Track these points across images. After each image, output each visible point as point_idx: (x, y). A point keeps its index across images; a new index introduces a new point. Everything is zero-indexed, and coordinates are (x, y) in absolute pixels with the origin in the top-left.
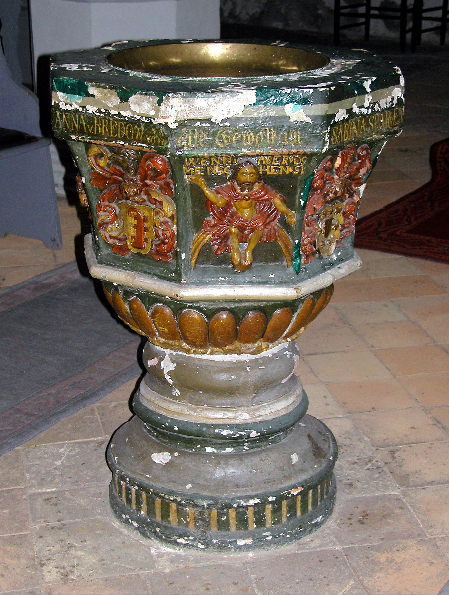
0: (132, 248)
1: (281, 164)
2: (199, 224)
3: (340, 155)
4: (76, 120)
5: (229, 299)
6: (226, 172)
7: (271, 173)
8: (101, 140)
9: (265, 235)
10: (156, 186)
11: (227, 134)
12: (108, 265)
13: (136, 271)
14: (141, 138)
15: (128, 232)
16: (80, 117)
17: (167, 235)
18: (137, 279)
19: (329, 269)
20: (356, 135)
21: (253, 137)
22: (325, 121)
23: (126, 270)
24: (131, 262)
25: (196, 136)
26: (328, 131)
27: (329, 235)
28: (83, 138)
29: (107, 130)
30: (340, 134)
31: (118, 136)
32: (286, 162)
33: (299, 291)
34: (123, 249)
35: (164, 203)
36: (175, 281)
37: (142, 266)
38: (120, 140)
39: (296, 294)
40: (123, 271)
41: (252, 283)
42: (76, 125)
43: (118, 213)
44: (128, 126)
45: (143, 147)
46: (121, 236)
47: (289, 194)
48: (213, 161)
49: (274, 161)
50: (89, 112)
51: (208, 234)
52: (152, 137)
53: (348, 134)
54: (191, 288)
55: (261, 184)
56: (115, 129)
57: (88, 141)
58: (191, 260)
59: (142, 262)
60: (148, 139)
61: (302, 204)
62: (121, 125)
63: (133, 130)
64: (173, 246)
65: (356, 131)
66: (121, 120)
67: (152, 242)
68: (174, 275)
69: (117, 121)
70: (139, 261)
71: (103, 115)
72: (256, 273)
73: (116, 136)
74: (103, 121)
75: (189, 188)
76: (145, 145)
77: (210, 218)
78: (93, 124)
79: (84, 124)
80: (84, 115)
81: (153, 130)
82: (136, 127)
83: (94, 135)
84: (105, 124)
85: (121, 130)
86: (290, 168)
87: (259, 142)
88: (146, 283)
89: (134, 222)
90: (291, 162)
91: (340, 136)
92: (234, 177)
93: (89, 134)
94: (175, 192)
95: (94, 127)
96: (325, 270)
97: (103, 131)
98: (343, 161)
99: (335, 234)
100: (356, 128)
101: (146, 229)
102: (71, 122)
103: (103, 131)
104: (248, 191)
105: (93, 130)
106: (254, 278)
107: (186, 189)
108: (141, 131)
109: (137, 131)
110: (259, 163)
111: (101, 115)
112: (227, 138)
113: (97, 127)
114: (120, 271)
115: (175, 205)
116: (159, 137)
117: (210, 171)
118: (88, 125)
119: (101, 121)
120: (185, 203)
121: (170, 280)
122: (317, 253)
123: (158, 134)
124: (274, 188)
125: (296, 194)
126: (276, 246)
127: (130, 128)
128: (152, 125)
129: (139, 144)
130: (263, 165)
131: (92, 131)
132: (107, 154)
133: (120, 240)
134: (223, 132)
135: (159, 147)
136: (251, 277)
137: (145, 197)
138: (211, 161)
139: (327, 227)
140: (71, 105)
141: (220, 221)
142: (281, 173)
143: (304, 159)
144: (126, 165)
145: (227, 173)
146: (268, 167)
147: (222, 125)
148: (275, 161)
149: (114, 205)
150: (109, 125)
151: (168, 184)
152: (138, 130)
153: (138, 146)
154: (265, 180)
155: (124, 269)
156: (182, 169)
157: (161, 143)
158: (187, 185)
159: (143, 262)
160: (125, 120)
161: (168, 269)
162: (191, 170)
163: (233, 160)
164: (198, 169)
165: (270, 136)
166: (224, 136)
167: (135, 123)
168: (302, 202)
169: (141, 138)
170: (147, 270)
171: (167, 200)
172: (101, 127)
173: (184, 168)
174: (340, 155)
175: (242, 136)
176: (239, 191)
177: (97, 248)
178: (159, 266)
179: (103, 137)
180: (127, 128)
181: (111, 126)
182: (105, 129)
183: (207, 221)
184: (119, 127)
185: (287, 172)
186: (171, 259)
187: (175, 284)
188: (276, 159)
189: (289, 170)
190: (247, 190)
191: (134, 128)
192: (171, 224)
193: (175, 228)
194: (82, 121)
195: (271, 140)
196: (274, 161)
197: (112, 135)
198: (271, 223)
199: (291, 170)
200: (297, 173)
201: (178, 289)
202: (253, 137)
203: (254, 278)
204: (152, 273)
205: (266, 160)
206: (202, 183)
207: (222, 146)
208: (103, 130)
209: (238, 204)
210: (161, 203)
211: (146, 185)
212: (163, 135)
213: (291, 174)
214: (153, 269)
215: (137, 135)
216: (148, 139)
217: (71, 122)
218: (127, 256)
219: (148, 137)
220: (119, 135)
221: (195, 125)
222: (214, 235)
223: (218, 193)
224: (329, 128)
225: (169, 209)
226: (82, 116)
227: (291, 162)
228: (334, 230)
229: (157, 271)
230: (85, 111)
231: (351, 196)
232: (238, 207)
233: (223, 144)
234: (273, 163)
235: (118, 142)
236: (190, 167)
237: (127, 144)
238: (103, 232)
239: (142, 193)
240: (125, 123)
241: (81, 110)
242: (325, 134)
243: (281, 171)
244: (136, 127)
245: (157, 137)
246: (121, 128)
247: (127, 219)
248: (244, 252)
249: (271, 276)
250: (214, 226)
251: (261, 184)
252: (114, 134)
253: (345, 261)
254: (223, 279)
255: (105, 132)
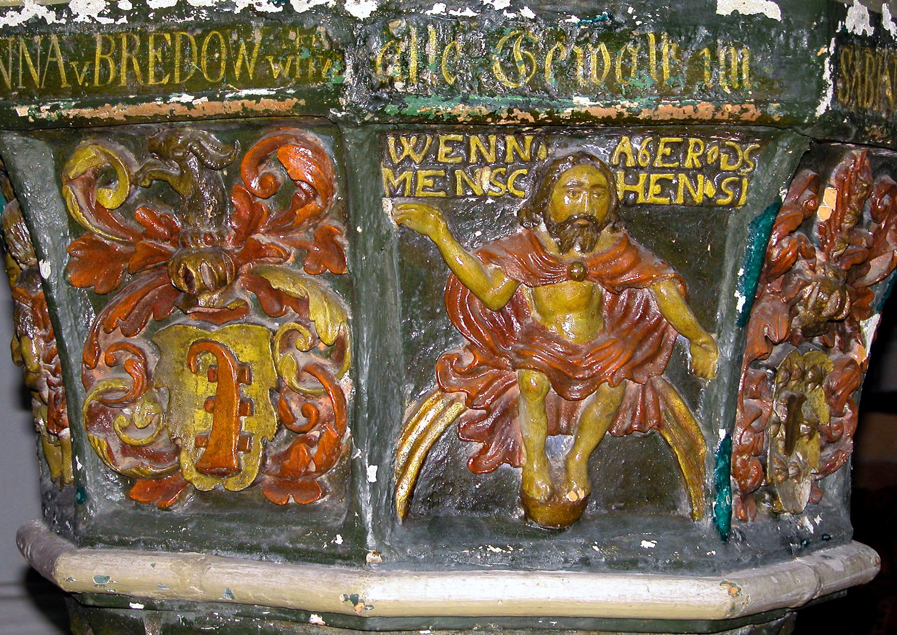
0: (195, 475)
1: (679, 170)
2: (420, 366)
3: (833, 181)
4: (33, 57)
5: (520, 612)
6: (512, 190)
7: (651, 199)
8: (113, 103)
9: (626, 410)
10: (288, 250)
11: (527, 44)
12: (112, 544)
13: (210, 548)
14: (251, 71)
15: (184, 427)
16: (49, 42)
17: (318, 412)
18: (216, 566)
19: (799, 553)
20: (889, 104)
21: (607, 57)
22: (822, 19)
23: (175, 550)
24: (190, 526)
25: (431, 48)
26: (832, 51)
27: (794, 454)
28: (54, 108)
29: (137, 68)
30: (857, 77)
31: (172, 79)
32: (696, 162)
33: (734, 590)
34: (167, 485)
35: (314, 301)
36: (344, 559)
37: (228, 532)
38: (179, 90)
39: (729, 600)
40: (165, 555)
41: (586, 565)
42: (32, 70)
43: (152, 367)
44: (207, 39)
45: (257, 98)
46: (161, 446)
47: (699, 275)
48: (473, 149)
49: (659, 157)
50: (79, 20)
51: (452, 403)
52: (290, 59)
53: (872, 90)
54: (399, 575)
55: (620, 235)
56: (164, 58)
57: (72, 113)
58: (396, 490)
59: (230, 519)
60: (276, 69)
61: (739, 308)
62: (186, 41)
63: (224, 50)
64: (337, 442)
65: (889, 93)
66: (185, 27)
67: (265, 447)
68: (339, 540)
69: (170, 32)
70: (221, 519)
71: (124, 20)
72: (597, 535)
73: (165, 81)
74: (124, 40)
75: (395, 247)
76: (264, 92)
77: (458, 348)
78: (91, 56)
79: (61, 61)
80: (60, 35)
81: (292, 35)
82: (235, 37)
83: (91, 91)
84: (131, 48)
85: (184, 57)
86: (709, 182)
87: (626, 72)
88: (248, 575)
89: (204, 388)
90: (710, 161)
91: (856, 84)
92: (540, 202)
93: (76, 92)
94: (354, 255)
95: (93, 65)
96: (790, 554)
97: (123, 74)
98: (841, 203)
99: (808, 450)
100: (889, 83)
101: (246, 407)
102: (16, 63)
103: (123, 74)
104: (583, 250)
105: (90, 77)
106: (596, 548)
107: (387, 247)
108: (250, 47)
109: (239, 46)
110: (615, 161)
111: (119, 22)
112: (526, 60)
113: (104, 63)
114: (156, 555)
115: (347, 308)
116: (313, 55)
117: (465, 185)
118: (74, 64)
119: (119, 42)
120: (383, 294)
121: (328, 558)
122: (767, 496)
123: (309, 47)
124: (656, 252)
125: (720, 275)
126: (656, 451)
127: (214, 45)
128: (290, 21)
129: (244, 93)
130: (626, 170)
131: (85, 81)
132: (128, 164)
133: (155, 457)
134: (514, 38)
135: (314, 86)
136: (586, 546)
137: (247, 297)
138: (468, 150)
139: (791, 420)
140: (19, 9)
141: (491, 355)
142: (680, 200)
143: (752, 153)
144: (190, 186)
145: (516, 193)
146: (643, 176)
147: (511, 16)
148: (664, 155)
149: (136, 340)
150: (144, 48)
151: (327, 239)
152: (243, 47)
153: (240, 98)
154: (628, 221)
155: (168, 548)
156: (379, 174)
157: (319, 73)
158: (388, 232)
159: (231, 519)
160: (199, 24)
161: (319, 527)
162: (405, 180)
163: (537, 149)
164: (428, 177)
165: (659, 56)
166: (518, 53)
167: (233, 26)
168: (742, 301)
169: (251, 71)
170: (245, 539)
171: (324, 293)
172: (117, 61)
173: (386, 172)
174: (833, 181)
175: (573, 55)
176: (553, 251)
177: (79, 496)
178: (287, 523)
179: (125, 91)
180: (205, 48)
181: (152, 53)
182: (130, 65)
183: (450, 358)
184: (178, 48)
185: (698, 198)
186: (326, 499)
187: (344, 568)
188: (668, 151)
189: (706, 189)
190: (577, 248)
191: (227, 43)
192: (332, 370)
193: (346, 383)
194: (54, 55)
195: (660, 72)
196: (659, 157)
197: (152, 81)
198: (646, 367)
199: (710, 190)
200: (728, 200)
201: (358, 579)
202: (607, 57)
203: (596, 548)
204: (264, 546)
205: (636, 153)
206: (436, 228)
207: (512, 86)
208: (124, 69)
209: (549, 297)
210: (301, 304)
211: (258, 251)
212: (327, 46)
213: (709, 202)
214: (265, 536)
215: (239, 63)
216: (276, 69)
217: (16, 63)
218: (178, 510)
219: (276, 61)
220: (177, 74)
221: (428, 13)
222: (470, 402)
223: (489, 257)
224: (833, 44)
225: (327, 320)
226: (54, 38)
227: (710, 161)
228: (805, 439)
229: (283, 537)
230: (63, 21)
231: (845, 347)
232: (549, 306)
233: (516, 78)
234: (658, 163)
235: (174, 99)
236: (403, 170)
237: (205, 99)
238: (102, 435)
239: (238, 285)
240: (199, 31)
241: (51, 17)
242: (821, 59)
243: (681, 192)
244: (235, 37)
245: (306, 54)
246: (183, 51)
247: (182, 385)
248: (560, 464)
249: (646, 544)
250: (472, 371)
251: (620, 235)
252: (158, 76)
253: (835, 545)
254: (498, 550)
255: (132, 76)
